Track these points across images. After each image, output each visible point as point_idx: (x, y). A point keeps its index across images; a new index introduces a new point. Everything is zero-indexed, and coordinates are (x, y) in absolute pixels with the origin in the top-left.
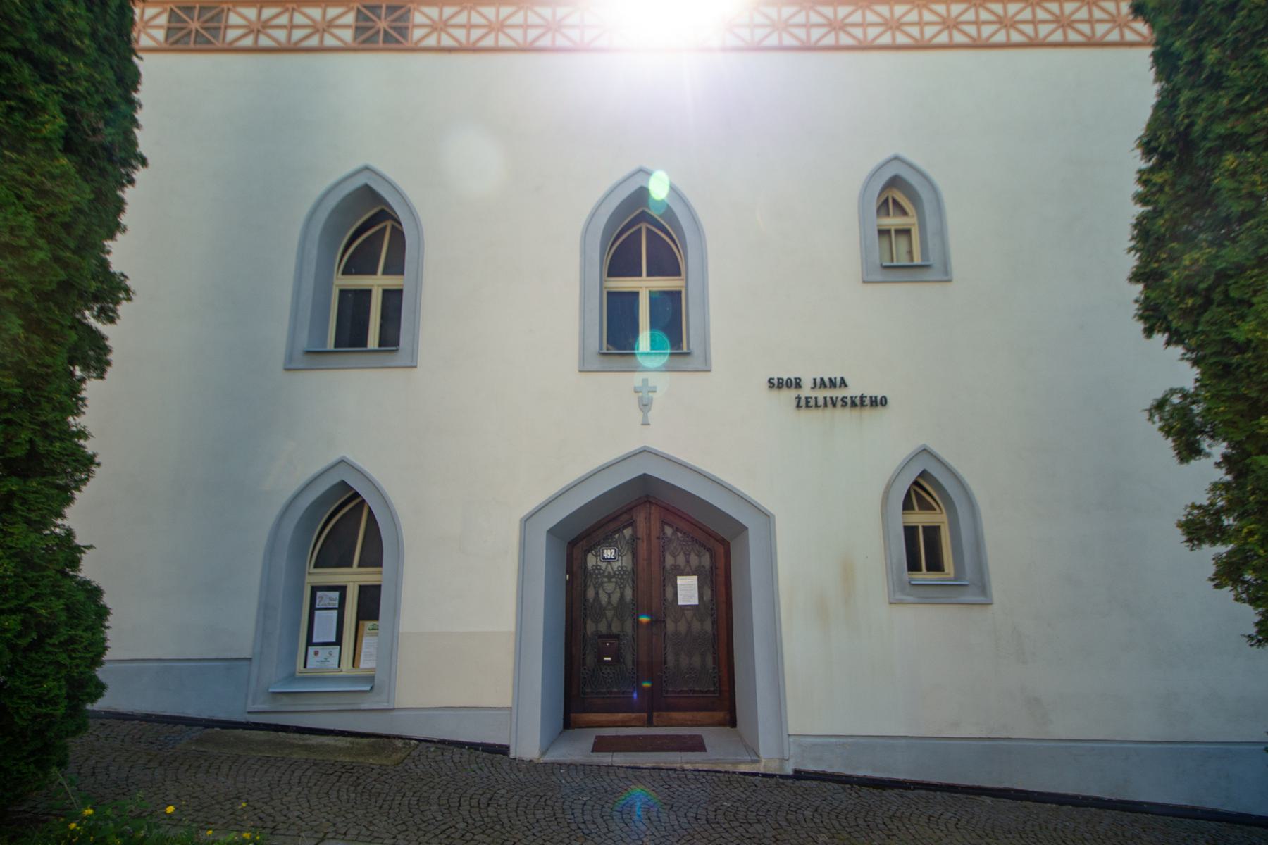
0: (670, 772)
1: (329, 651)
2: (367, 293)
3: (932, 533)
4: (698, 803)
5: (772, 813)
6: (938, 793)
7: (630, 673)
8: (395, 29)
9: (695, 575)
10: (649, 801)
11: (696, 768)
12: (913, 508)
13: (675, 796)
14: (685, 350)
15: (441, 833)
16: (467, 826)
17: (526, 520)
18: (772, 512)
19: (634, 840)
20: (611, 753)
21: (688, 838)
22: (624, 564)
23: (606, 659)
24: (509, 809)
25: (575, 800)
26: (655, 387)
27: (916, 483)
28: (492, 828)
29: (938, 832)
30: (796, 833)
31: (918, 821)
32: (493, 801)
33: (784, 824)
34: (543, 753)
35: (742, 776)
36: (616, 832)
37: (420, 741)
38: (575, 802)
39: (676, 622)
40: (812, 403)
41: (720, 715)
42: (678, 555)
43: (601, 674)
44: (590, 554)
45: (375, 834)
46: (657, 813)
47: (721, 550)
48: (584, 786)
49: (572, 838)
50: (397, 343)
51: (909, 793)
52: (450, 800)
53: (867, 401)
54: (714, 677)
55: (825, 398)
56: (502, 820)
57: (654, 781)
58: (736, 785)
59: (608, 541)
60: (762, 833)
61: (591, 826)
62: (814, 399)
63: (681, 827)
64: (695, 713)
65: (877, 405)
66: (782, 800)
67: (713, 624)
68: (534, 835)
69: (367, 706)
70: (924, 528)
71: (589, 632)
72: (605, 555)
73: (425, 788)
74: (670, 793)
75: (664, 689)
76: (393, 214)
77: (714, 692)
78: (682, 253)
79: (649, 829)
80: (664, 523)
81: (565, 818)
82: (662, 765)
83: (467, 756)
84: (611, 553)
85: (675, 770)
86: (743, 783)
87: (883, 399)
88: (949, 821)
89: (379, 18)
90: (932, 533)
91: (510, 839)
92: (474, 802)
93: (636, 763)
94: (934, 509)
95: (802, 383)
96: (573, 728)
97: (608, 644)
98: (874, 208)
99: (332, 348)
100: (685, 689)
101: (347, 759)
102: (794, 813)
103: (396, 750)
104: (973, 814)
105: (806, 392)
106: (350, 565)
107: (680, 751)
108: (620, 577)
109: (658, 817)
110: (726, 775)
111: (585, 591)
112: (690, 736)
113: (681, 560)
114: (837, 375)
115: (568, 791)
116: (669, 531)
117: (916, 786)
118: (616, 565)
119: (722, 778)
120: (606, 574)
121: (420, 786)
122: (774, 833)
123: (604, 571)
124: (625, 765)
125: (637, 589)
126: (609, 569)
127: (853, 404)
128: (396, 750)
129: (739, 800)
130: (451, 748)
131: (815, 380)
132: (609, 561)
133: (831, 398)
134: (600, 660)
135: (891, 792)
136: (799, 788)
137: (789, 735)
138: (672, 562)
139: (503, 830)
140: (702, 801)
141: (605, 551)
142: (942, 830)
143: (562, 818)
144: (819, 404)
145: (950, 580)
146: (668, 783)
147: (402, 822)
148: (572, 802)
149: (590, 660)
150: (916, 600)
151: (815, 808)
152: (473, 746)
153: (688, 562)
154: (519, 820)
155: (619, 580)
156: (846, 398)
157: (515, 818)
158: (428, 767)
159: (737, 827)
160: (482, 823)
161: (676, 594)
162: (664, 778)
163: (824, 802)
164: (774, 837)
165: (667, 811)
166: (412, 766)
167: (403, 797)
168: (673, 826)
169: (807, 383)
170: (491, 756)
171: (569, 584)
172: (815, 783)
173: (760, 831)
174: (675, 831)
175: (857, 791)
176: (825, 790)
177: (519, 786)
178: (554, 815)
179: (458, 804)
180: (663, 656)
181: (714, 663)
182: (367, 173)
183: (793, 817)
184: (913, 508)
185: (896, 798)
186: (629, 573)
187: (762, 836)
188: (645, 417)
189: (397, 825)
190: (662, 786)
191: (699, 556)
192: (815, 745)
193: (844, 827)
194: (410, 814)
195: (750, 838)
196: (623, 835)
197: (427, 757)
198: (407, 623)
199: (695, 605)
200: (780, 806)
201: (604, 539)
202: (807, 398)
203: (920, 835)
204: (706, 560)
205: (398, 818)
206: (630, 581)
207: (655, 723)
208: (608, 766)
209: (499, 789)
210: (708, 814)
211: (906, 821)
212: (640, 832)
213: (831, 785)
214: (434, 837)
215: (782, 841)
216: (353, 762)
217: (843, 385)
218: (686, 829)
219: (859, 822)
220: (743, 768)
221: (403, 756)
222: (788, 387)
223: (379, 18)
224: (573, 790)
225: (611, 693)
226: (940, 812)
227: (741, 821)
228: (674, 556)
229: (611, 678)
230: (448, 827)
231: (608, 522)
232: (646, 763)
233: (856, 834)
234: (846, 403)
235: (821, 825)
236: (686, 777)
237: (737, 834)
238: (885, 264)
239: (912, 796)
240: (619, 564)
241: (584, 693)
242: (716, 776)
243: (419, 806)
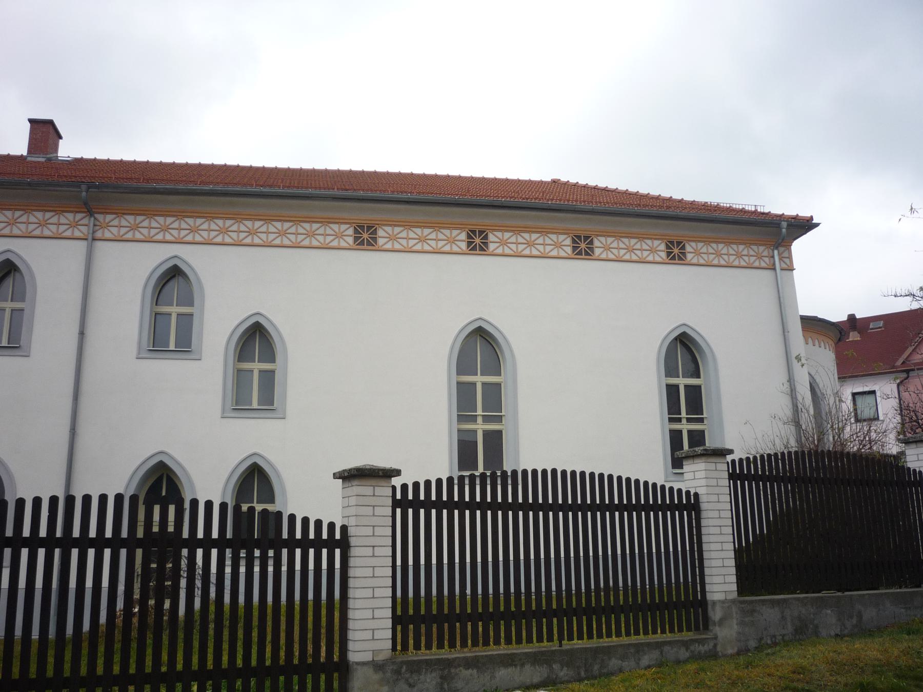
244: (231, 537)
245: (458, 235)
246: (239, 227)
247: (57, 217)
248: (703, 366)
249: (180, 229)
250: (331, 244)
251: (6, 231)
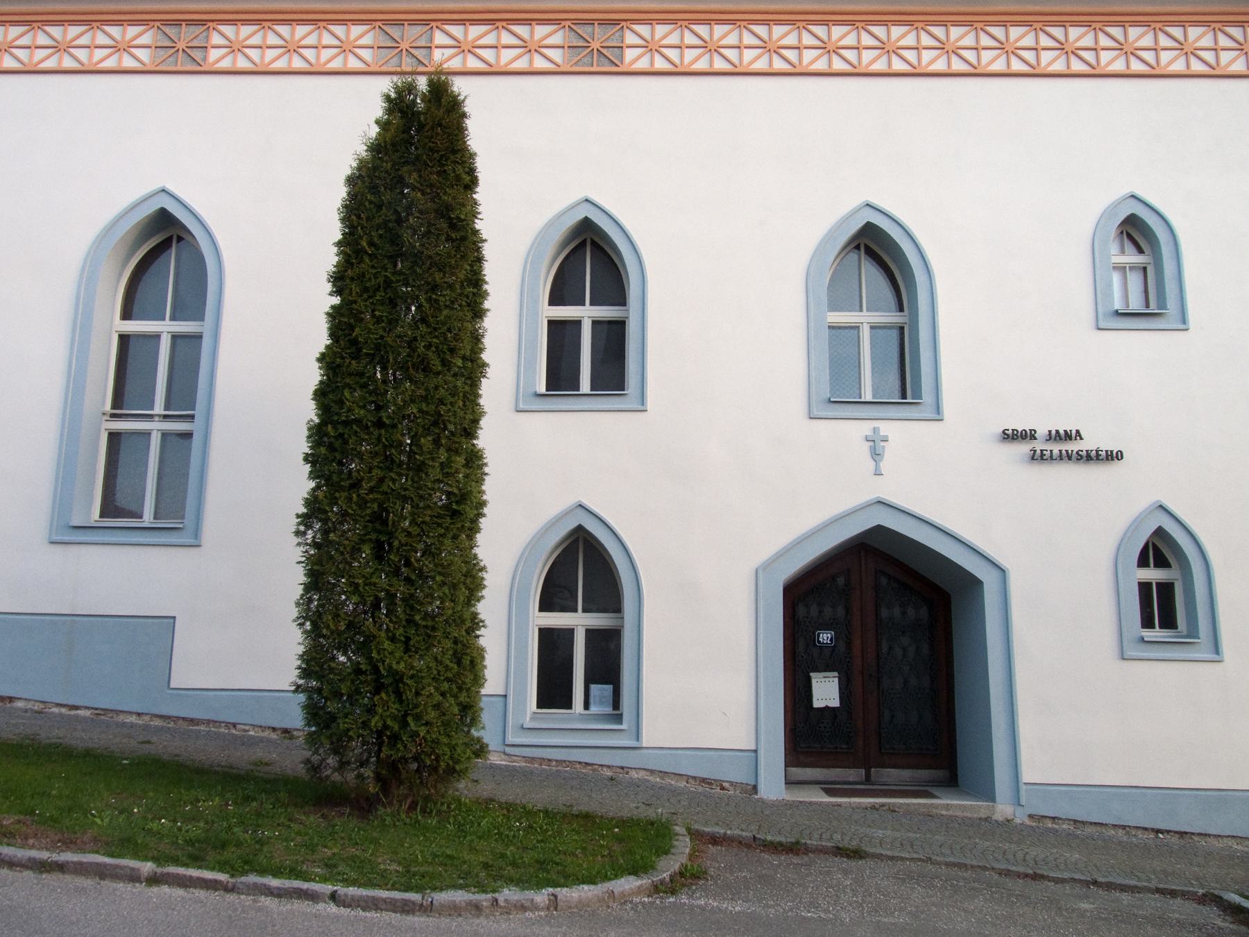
3: (1166, 589)
18: (1008, 566)
55: (1060, 451)
65: (1112, 459)
105: (1039, 446)
133: (1067, 451)
153: (904, 613)
202: (1042, 451)
217: (1078, 438)
244: (836, 674)
245: (903, 36)
246: (264, 38)
247: (854, 34)
248: (902, 275)
250: (812, 67)
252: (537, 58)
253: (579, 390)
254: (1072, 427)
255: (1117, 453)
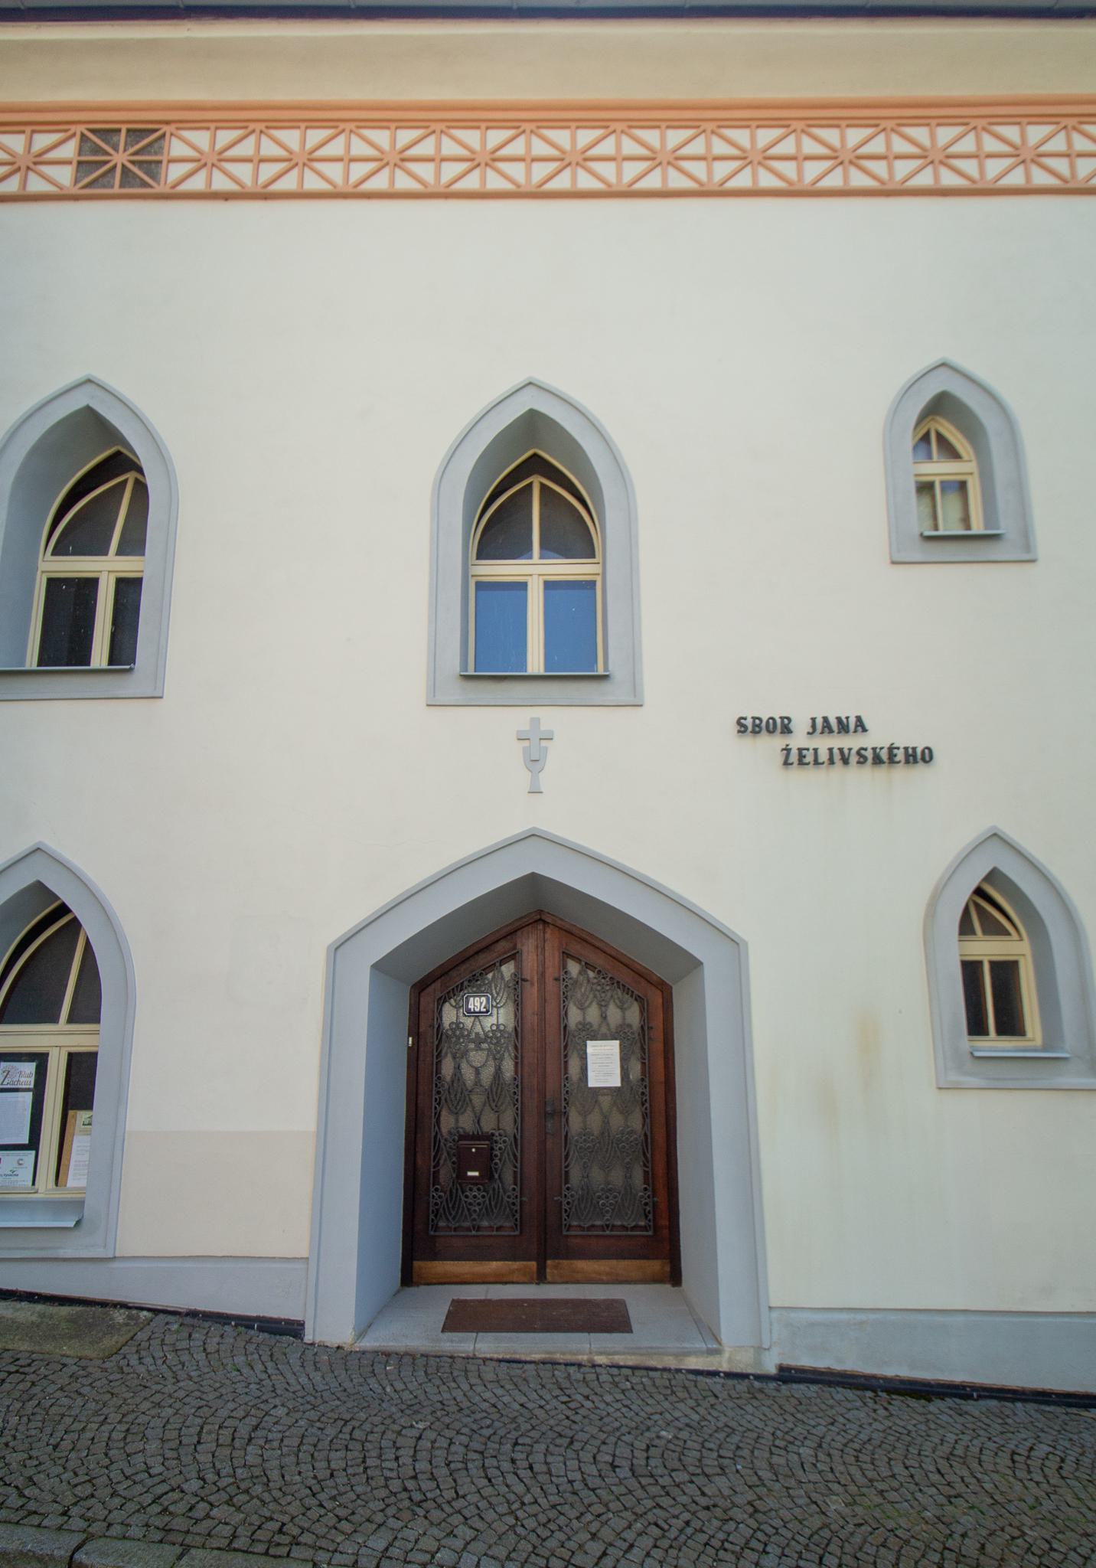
0: (571, 1370)
1: (18, 1158)
2: (91, 584)
3: (1006, 972)
4: (618, 1434)
5: (746, 1453)
6: (1019, 1405)
7: (509, 1197)
8: (139, 164)
9: (616, 1039)
10: (533, 1428)
11: (615, 1362)
12: (973, 932)
13: (577, 1418)
14: (601, 671)
15: (153, 1502)
16: (203, 1487)
17: (338, 948)
18: (744, 937)
19: (501, 1515)
20: (474, 1335)
21: (598, 1508)
22: (501, 1021)
23: (470, 1174)
24: (285, 1450)
25: (404, 1427)
26: (552, 732)
27: (979, 892)
28: (247, 1491)
29: (1031, 1484)
30: (790, 1496)
31: (995, 1464)
32: (259, 1433)
33: (766, 1475)
34: (361, 1334)
35: (691, 1377)
36: (468, 1497)
37: (156, 1311)
38: (404, 1432)
39: (584, 1114)
40: (809, 758)
41: (655, 1266)
42: (588, 1006)
43: (463, 1198)
44: (447, 1004)
45: (32, 1506)
46: (545, 1455)
47: (656, 999)
48: (422, 1397)
49: (391, 1511)
50: (132, 660)
51: (968, 1406)
52: (184, 1431)
53: (900, 755)
54: (646, 1204)
55: (831, 750)
56: (268, 1473)
57: (543, 1386)
58: (682, 1394)
59: (475, 982)
60: (729, 1496)
61: (427, 1485)
62: (811, 751)
63: (586, 1485)
64: (614, 1262)
65: (915, 761)
66: (761, 1425)
67: (644, 1118)
68: (321, 1505)
69: (69, 1253)
70: (993, 964)
71: (444, 1130)
72: (471, 1006)
73: (145, 1405)
74: (569, 1413)
75: (564, 1222)
76: (135, 460)
77: (645, 1228)
78: (598, 530)
79: (528, 1490)
80: (566, 955)
81: (382, 1469)
82: (558, 1357)
83: (232, 1340)
84: (481, 1003)
85: (580, 1365)
86: (693, 1389)
87: (927, 751)
88: (1047, 1463)
89: (116, 148)
90: (1006, 972)
91: (275, 1516)
92: (225, 1436)
93: (515, 1353)
94: (1008, 934)
95: (792, 726)
96: (418, 1284)
97: (474, 1150)
98: (909, 441)
99: (34, 667)
100: (598, 1223)
101: (25, 1346)
102: (783, 1452)
103: (113, 1328)
104: (1083, 1446)
105: (799, 739)
106: (54, 1019)
107: (589, 1332)
108: (494, 1041)
109: (546, 1463)
110: (666, 1375)
111: (439, 1063)
112: (605, 1300)
113: (593, 1014)
114: (850, 713)
115: (394, 1409)
116: (574, 968)
117: (982, 1393)
118: (489, 1022)
119: (658, 1382)
120: (473, 1036)
121: (138, 1400)
122: (750, 1496)
123: (470, 1033)
124: (495, 1356)
125: (522, 1062)
126: (478, 1029)
127: (877, 760)
128: (113, 1328)
129: (687, 1425)
130: (207, 1324)
131: (813, 720)
132: (477, 1015)
133: (841, 750)
134: (461, 1175)
135: (938, 1403)
136: (787, 1399)
137: (770, 1308)
138: (579, 1018)
139: (266, 1495)
140: (624, 1429)
141: (472, 999)
142: (1037, 1483)
143: (376, 1467)
144: (820, 761)
145: (1035, 1050)
146: (568, 1392)
147: (87, 1478)
148: (399, 1433)
149: (446, 1173)
150: (983, 1083)
151: (817, 1439)
152: (245, 1322)
153: (604, 1017)
154: (300, 1473)
155: (493, 1047)
156: (866, 749)
157: (293, 1468)
158: (159, 1362)
159: (684, 1483)
160: (232, 1480)
161: (584, 1070)
162: (560, 1380)
163: (833, 1428)
164: (750, 1503)
165: (562, 1450)
166: (134, 1361)
167: (102, 1423)
168: (571, 1482)
169: (800, 726)
170: (273, 1339)
171: (414, 1058)
172: (814, 1388)
173: (727, 1492)
174: (575, 1493)
175: (885, 1404)
176: (831, 1402)
177: (310, 1398)
178: (364, 1462)
179: (195, 1440)
180: (564, 1169)
181: (646, 1181)
182: (89, 388)
183: (782, 1461)
184: (973, 932)
185: (951, 1416)
186: (510, 1034)
187: (728, 1504)
188: (535, 780)
189: (76, 1486)
190: (557, 1397)
191: (622, 1009)
192: (812, 1325)
193: (871, 1481)
194: (107, 1461)
195: (707, 1508)
196: (483, 1504)
197: (163, 1343)
198: (138, 1117)
199: (616, 1087)
200: (758, 1437)
201: (469, 981)
202: (800, 750)
203: (1002, 1493)
204: (634, 1016)
205: (81, 1471)
206: (511, 1048)
207: (549, 1277)
208: (468, 1358)
209: (275, 1407)
210: (633, 1457)
211: (975, 1465)
212: (512, 1497)
213: (841, 1393)
214: (138, 1511)
215: (764, 1513)
216: (33, 1353)
217: (860, 729)
218: (593, 1490)
219: (896, 1471)
220: (694, 1363)
221: (122, 1340)
222: (769, 731)
223: (116, 148)
224: (404, 1407)
225: (479, 1229)
226: (1028, 1444)
227: (691, 1469)
228: (582, 1008)
229: (479, 1204)
230: (168, 1488)
231: (477, 953)
232: (530, 1353)
233: (892, 1496)
234: (865, 759)
235: (830, 1476)
236: (598, 1379)
237: (684, 1499)
238: (927, 533)
239: (977, 1413)
240: (492, 1020)
241: (436, 1228)
242: (648, 1376)
243: (126, 1444)
249: (441, 160)
251: (12, 186)
252: (1036, 171)
253: (89, 664)
254: (849, 712)
255: (923, 752)
